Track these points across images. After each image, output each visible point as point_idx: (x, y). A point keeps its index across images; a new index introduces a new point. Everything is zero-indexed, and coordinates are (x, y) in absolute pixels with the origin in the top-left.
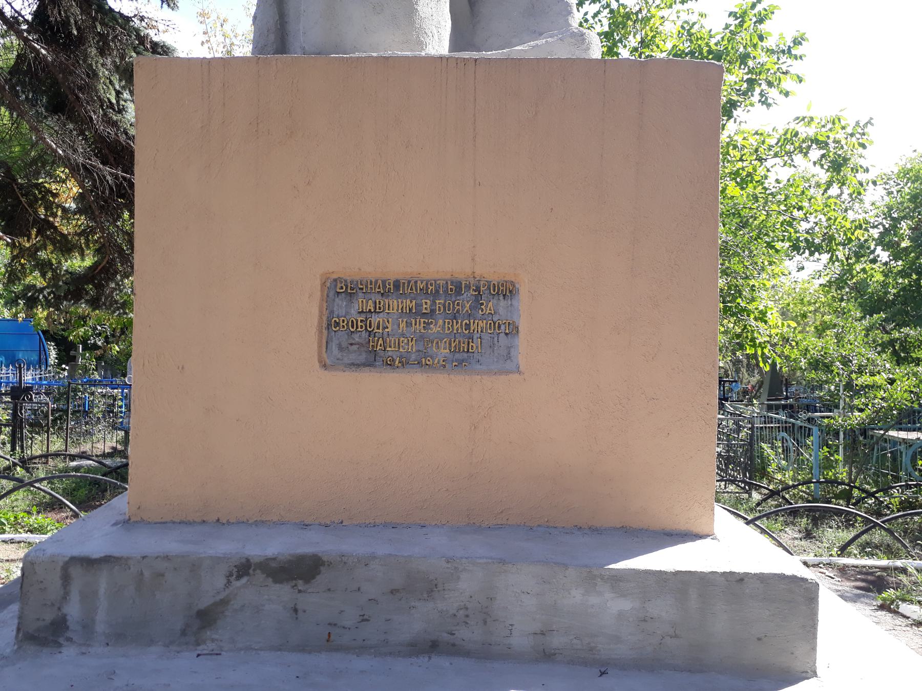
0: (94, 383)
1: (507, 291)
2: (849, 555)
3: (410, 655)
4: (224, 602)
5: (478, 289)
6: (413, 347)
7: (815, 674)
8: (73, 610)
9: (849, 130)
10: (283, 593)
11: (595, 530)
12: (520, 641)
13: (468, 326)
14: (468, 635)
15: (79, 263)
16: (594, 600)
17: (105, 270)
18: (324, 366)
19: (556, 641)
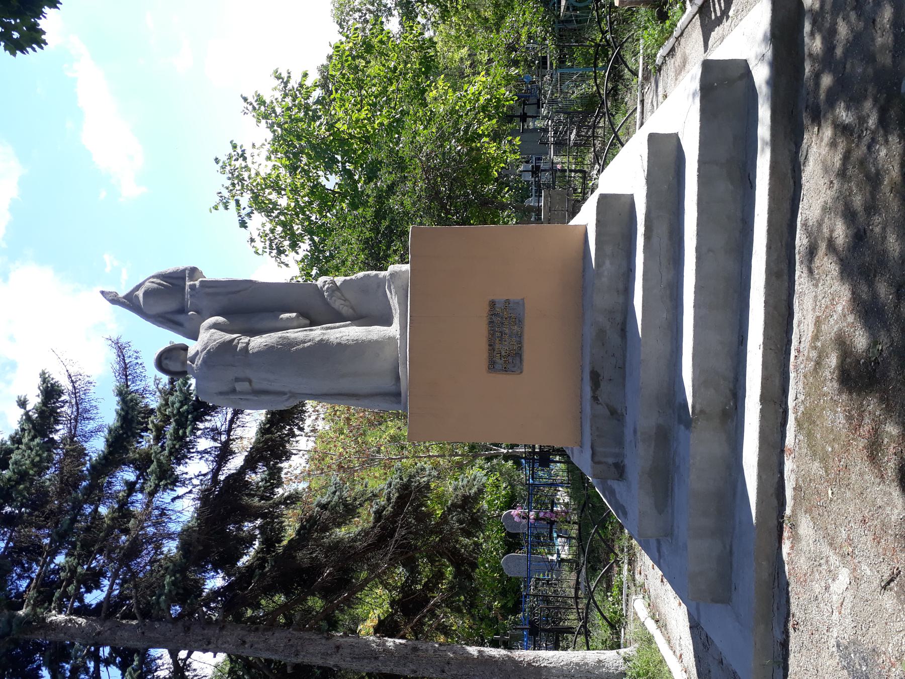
2: (638, 71)
3: (626, 338)
4: (607, 406)
5: (492, 315)
6: (514, 339)
7: (632, 195)
8: (611, 460)
9: (344, 39)
10: (604, 385)
11: (584, 271)
13: (506, 318)
14: (619, 318)
15: (449, 571)
16: (606, 273)
17: (453, 554)
18: (521, 372)
19: (621, 286)
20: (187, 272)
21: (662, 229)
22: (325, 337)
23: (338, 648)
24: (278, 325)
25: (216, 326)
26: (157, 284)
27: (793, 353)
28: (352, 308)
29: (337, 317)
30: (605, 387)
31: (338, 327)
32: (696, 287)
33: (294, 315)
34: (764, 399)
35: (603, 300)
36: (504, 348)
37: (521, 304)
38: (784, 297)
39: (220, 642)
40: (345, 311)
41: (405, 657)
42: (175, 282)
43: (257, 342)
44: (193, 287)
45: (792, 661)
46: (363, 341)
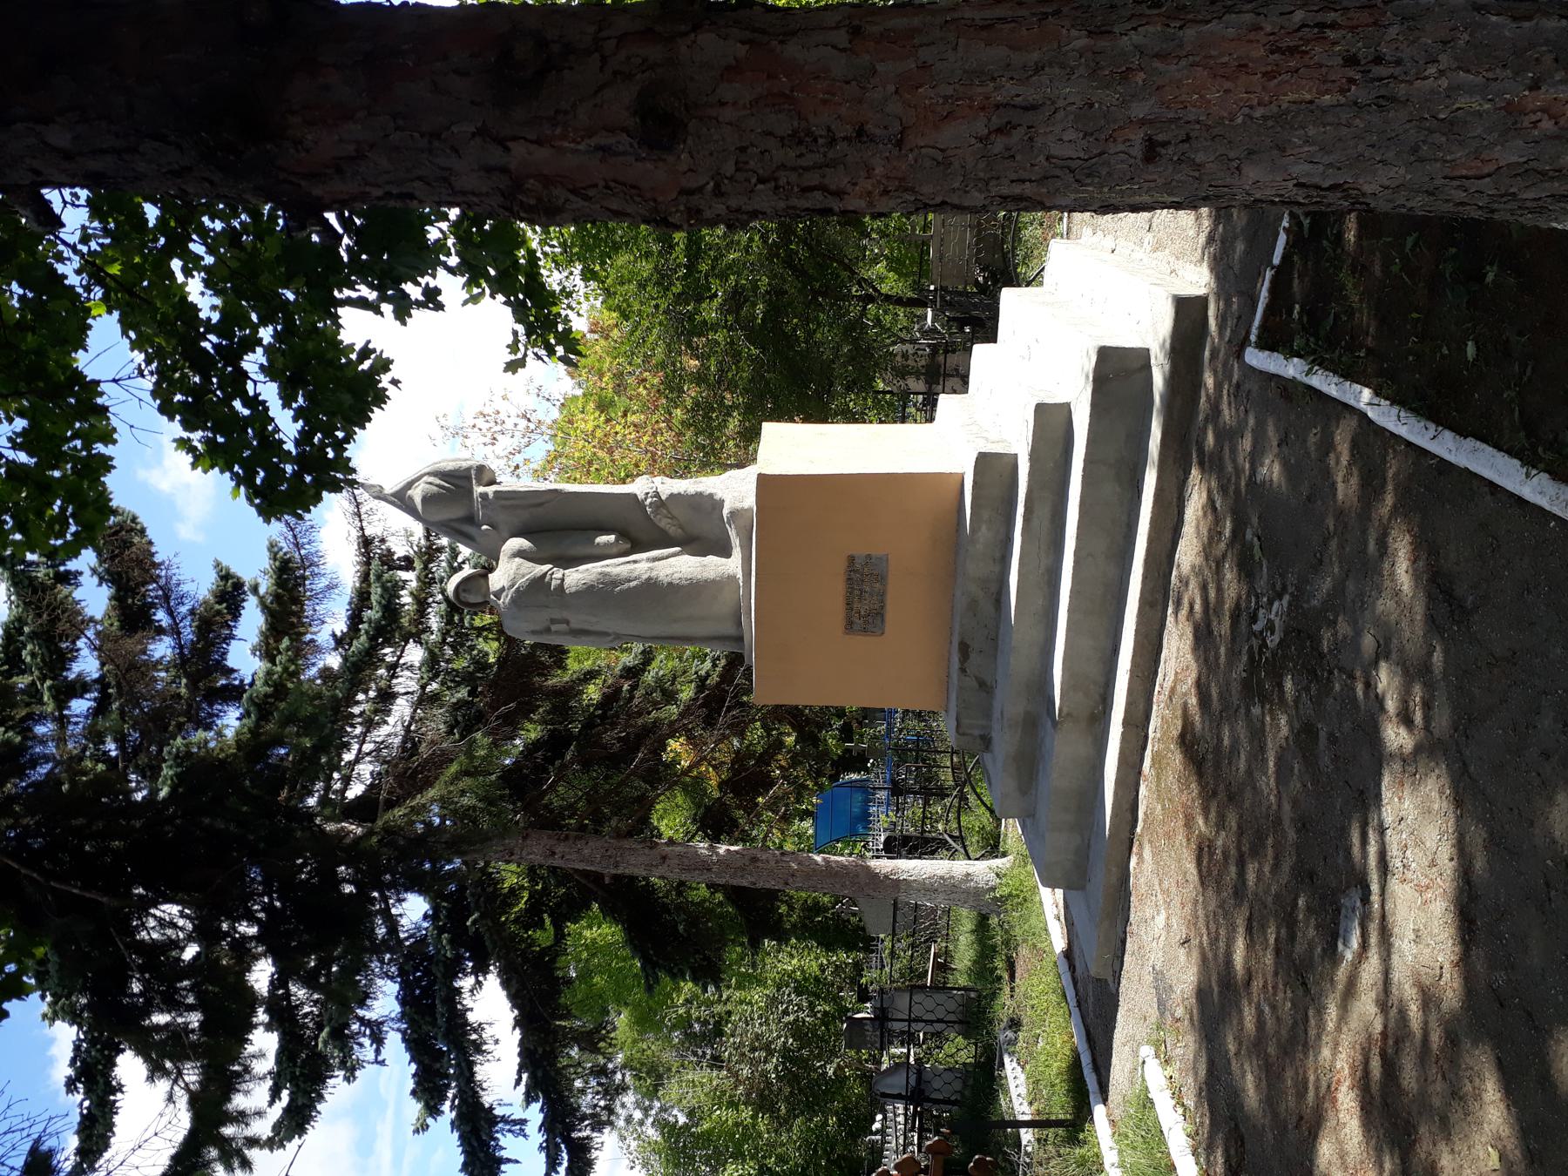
0: (890, 730)
1: (852, 559)
7: (1068, 405)
8: (977, 732)
10: (973, 656)
12: (997, 569)
17: (795, 717)
19: (998, 555)
20: (473, 472)
21: (1044, 512)
22: (654, 574)
23: (664, 858)
24: (596, 551)
25: (520, 554)
26: (437, 486)
27: (1157, 688)
28: (681, 527)
29: (663, 540)
30: (974, 658)
31: (667, 557)
32: (1072, 591)
33: (612, 538)
34: (1126, 723)
35: (976, 568)
36: (863, 607)
37: (884, 560)
38: (1156, 627)
39: (524, 853)
40: (673, 531)
41: (743, 869)
42: (457, 482)
43: (576, 577)
44: (484, 496)
45: (1127, 958)
46: (698, 582)
